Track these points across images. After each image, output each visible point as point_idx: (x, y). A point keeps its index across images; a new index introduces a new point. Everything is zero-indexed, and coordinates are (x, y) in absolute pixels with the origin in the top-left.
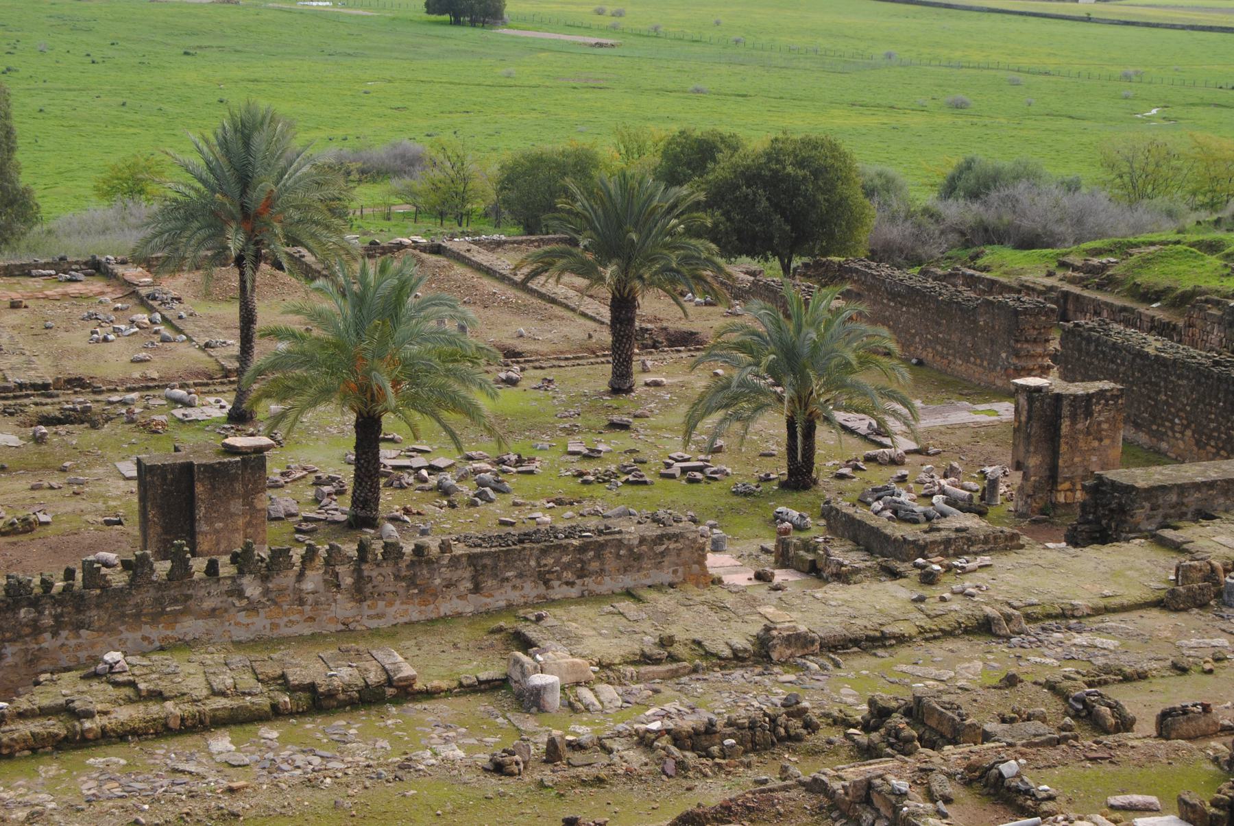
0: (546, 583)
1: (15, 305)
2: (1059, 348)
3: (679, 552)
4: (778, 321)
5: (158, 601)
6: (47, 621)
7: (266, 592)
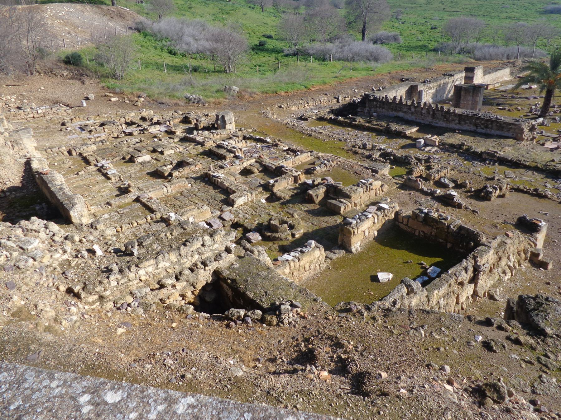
0: (477, 127)
1: (336, 77)
3: (515, 129)
5: (396, 107)
6: (378, 105)
7: (415, 111)
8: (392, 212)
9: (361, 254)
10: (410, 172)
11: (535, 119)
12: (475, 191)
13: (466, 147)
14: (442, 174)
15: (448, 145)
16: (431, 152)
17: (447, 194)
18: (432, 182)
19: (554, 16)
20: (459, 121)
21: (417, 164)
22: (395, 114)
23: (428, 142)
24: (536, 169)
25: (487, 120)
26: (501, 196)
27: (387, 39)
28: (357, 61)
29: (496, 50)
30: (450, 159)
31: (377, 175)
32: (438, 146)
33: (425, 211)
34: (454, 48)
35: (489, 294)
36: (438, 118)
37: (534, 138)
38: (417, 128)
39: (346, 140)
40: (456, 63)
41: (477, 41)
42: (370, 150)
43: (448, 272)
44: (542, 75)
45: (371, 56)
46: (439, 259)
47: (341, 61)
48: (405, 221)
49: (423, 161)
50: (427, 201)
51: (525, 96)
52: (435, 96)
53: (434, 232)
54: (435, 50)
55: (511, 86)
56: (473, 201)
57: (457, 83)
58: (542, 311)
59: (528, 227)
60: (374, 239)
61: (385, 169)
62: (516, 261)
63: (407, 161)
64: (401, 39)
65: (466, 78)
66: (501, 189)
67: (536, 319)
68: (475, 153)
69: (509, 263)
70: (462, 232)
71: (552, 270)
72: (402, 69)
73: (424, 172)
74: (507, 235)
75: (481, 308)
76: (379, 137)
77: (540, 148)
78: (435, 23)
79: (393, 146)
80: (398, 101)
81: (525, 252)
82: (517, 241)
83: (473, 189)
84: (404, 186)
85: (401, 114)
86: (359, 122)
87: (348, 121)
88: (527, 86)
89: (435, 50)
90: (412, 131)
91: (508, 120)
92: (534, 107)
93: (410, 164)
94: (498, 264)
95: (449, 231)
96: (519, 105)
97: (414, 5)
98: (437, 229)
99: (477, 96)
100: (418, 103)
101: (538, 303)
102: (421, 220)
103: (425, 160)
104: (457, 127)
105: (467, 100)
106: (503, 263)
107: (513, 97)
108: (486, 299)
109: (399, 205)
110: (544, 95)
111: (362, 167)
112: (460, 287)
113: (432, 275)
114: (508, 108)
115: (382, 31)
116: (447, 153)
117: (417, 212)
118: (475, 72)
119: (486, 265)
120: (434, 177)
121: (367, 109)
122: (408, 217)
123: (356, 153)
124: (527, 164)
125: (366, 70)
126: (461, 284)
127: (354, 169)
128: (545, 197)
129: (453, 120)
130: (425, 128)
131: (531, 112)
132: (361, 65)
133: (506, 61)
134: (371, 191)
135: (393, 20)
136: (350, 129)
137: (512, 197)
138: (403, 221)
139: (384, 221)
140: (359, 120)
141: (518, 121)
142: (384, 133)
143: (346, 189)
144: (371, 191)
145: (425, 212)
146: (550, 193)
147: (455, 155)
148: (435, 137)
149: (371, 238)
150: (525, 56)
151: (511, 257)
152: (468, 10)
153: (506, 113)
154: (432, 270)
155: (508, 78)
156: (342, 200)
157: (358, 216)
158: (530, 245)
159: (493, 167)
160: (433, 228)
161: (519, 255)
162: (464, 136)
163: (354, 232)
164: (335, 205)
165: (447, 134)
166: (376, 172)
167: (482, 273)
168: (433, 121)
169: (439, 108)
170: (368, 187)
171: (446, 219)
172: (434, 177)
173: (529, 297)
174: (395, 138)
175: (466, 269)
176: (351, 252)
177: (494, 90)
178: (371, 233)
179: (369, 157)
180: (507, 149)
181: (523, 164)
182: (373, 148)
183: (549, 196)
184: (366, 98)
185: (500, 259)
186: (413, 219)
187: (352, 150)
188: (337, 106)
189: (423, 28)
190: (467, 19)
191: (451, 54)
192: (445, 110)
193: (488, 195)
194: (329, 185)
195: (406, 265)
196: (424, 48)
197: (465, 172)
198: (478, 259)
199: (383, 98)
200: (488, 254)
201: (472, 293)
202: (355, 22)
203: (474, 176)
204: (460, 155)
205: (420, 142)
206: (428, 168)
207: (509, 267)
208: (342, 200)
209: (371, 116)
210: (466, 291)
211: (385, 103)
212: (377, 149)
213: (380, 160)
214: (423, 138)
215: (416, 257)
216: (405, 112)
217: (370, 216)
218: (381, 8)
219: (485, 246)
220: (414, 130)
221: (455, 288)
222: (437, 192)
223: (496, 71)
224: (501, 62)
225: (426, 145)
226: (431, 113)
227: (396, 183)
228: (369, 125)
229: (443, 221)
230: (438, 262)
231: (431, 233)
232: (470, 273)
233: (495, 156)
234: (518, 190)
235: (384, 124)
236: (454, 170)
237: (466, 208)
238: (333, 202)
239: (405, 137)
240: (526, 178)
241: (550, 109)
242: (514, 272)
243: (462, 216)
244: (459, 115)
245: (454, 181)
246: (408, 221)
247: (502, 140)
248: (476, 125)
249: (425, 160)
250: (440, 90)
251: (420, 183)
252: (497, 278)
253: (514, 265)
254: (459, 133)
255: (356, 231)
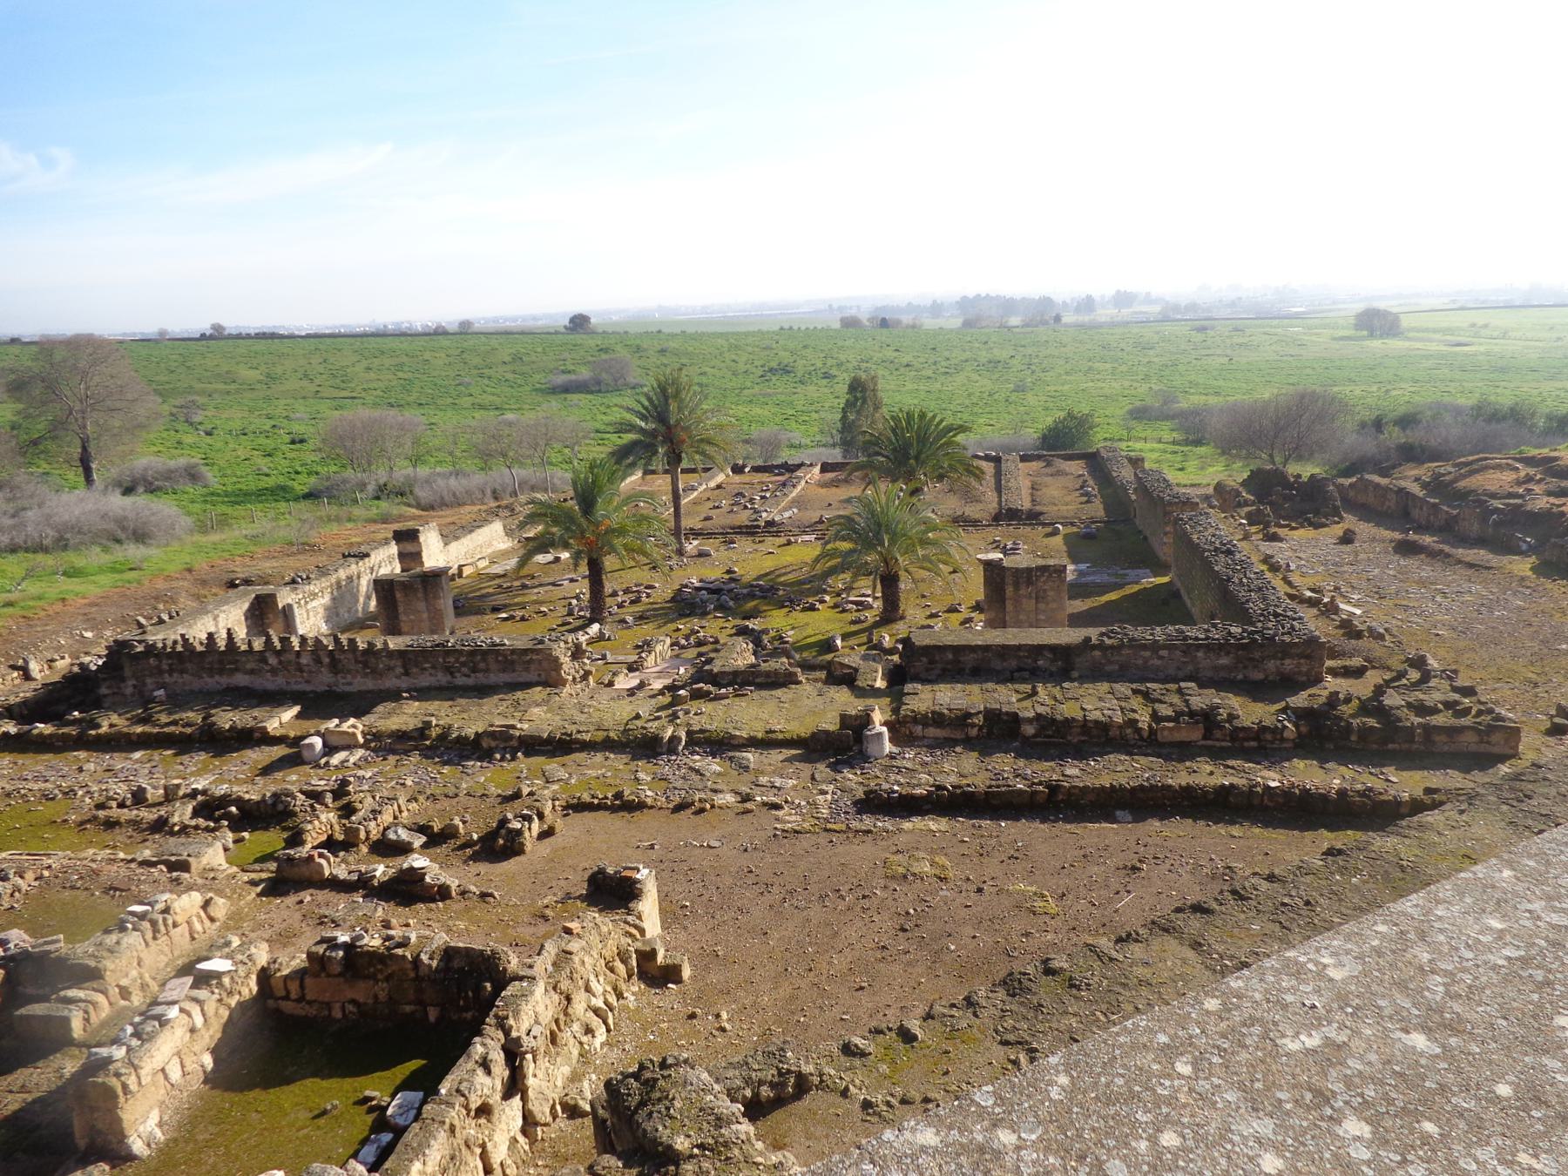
0: (452, 674)
1: (9, 604)
2: (241, 633)
3: (540, 662)
4: (1435, 456)
5: (221, 662)
6: (165, 667)
7: (280, 662)
8: (247, 976)
9: (166, 1154)
10: (296, 839)
11: (583, 628)
12: (480, 839)
13: (439, 731)
14: (387, 818)
15: (389, 736)
16: (350, 764)
17: (401, 871)
18: (364, 849)
19: (574, 398)
20: (404, 667)
21: (313, 809)
22: (224, 681)
23: (334, 741)
24: (608, 745)
25: (472, 653)
26: (547, 834)
27: (168, 478)
28: (76, 548)
29: (464, 482)
30: (404, 770)
31: (186, 875)
32: (365, 746)
33: (344, 938)
34: (362, 486)
35: (565, 1106)
36: (349, 671)
37: (587, 674)
38: (296, 709)
39: (69, 793)
40: (375, 521)
41: (415, 466)
42: (160, 804)
43: (437, 1092)
44: (567, 529)
45: (124, 529)
46: (415, 1064)
47: (21, 555)
48: (294, 987)
49: (329, 795)
50: (353, 906)
51: (551, 580)
52: (332, 613)
53: (382, 990)
54: (311, 496)
55: (512, 563)
56: (483, 867)
57: (384, 571)
58: (659, 1100)
59: (612, 892)
60: (205, 1082)
61: (210, 851)
62: (609, 989)
63: (280, 807)
64: (209, 475)
65: (402, 556)
66: (541, 816)
67: (648, 1126)
68: (462, 741)
69: (594, 1001)
70: (456, 964)
71: (693, 977)
72: (226, 555)
73: (337, 827)
74: (568, 931)
75: (556, 1155)
76: (185, 758)
77: (605, 694)
78: (298, 428)
79: (233, 776)
80: (222, 644)
81: (623, 956)
82: (594, 938)
83: (475, 837)
84: (276, 888)
85: (241, 680)
86: (111, 726)
87: (72, 731)
88: (549, 557)
89: (311, 496)
90: (282, 720)
91: (521, 644)
92: (574, 602)
93: (294, 814)
94: (566, 1014)
95: (421, 973)
96: (541, 603)
97: (233, 386)
98: (387, 979)
99: (436, 597)
100: (282, 640)
101: (647, 1081)
102: (338, 969)
103: (332, 791)
104: (404, 683)
105: (413, 609)
106: (579, 1006)
107: (524, 587)
108: (562, 1123)
109: (263, 945)
110: (584, 569)
111: (133, 865)
112: (482, 1121)
113: (401, 1121)
114: (519, 614)
115: (146, 460)
116: (392, 759)
117: (321, 949)
118: (422, 539)
119: (536, 1031)
120: (368, 833)
121: (131, 682)
122: (300, 974)
123: (110, 824)
124: (587, 737)
125: (113, 570)
126: (484, 1111)
127: (103, 878)
128: (641, 806)
129: (390, 669)
130: (316, 705)
131: (570, 614)
132: (94, 557)
133: (493, 504)
134: (173, 932)
135: (179, 427)
136: (82, 755)
137: (570, 830)
138: (288, 992)
139: (225, 1014)
140: (110, 722)
141: (542, 642)
142: (200, 742)
143: (82, 951)
144: (173, 932)
145: (345, 943)
146: (649, 793)
147: (415, 758)
148: (352, 721)
149: (196, 1083)
150: (533, 488)
151: (594, 985)
152: (379, 393)
153: (519, 625)
154: (400, 1106)
155: (505, 544)
156: (72, 993)
157: (130, 1030)
158: (631, 935)
159: (513, 764)
160: (377, 981)
161: (612, 970)
162: (425, 705)
163: (125, 1087)
164: (47, 1019)
165: (380, 708)
166: (184, 866)
167: (529, 1056)
168: (333, 682)
169: (345, 643)
170: (157, 924)
171: (404, 943)
172: (368, 833)
173: (626, 1076)
174: (237, 750)
175: (485, 1065)
176: (131, 1157)
177: (479, 575)
178: (189, 1068)
179: (160, 826)
180: (537, 715)
181: (577, 741)
182: (170, 795)
183: (649, 801)
184: (119, 653)
185: (568, 999)
186: (316, 975)
187: (95, 818)
188: (26, 692)
189: (269, 444)
190: (376, 413)
191: (355, 501)
192: (362, 646)
193: (513, 840)
194: (12, 958)
195: (322, 1121)
196: (280, 493)
197: (446, 796)
198: (511, 1021)
199: (175, 642)
200: (532, 1000)
201: (520, 1122)
202: (54, 438)
203: (471, 802)
204: (428, 753)
205: (311, 746)
206: (348, 811)
207: (596, 1011)
208: (72, 993)
209: (146, 701)
210: (503, 1126)
211: (185, 657)
212: (185, 796)
213: (196, 827)
214: (318, 733)
215: (348, 1083)
216: (252, 672)
217: (173, 1012)
218: (129, 396)
219: (521, 979)
220: (289, 714)
221: (470, 1129)
222: (378, 874)
223: (471, 532)
224: (484, 507)
225: (330, 749)
226: (326, 660)
227: (254, 883)
228: (147, 729)
229: (399, 951)
230: (414, 1074)
231: (376, 997)
232: (500, 1070)
233: (511, 737)
234: (579, 807)
235: (194, 716)
236: (416, 800)
237: (463, 893)
238: (38, 1009)
239: (268, 740)
240: (592, 773)
241: (609, 601)
242: (610, 1021)
243: (458, 919)
244: (401, 654)
245: (422, 829)
246: (302, 986)
247: (519, 694)
248: (449, 670)
249: (332, 791)
250: (342, 596)
251: (323, 861)
252: (575, 1052)
253: (606, 1003)
254: (411, 698)
255: (132, 1082)
